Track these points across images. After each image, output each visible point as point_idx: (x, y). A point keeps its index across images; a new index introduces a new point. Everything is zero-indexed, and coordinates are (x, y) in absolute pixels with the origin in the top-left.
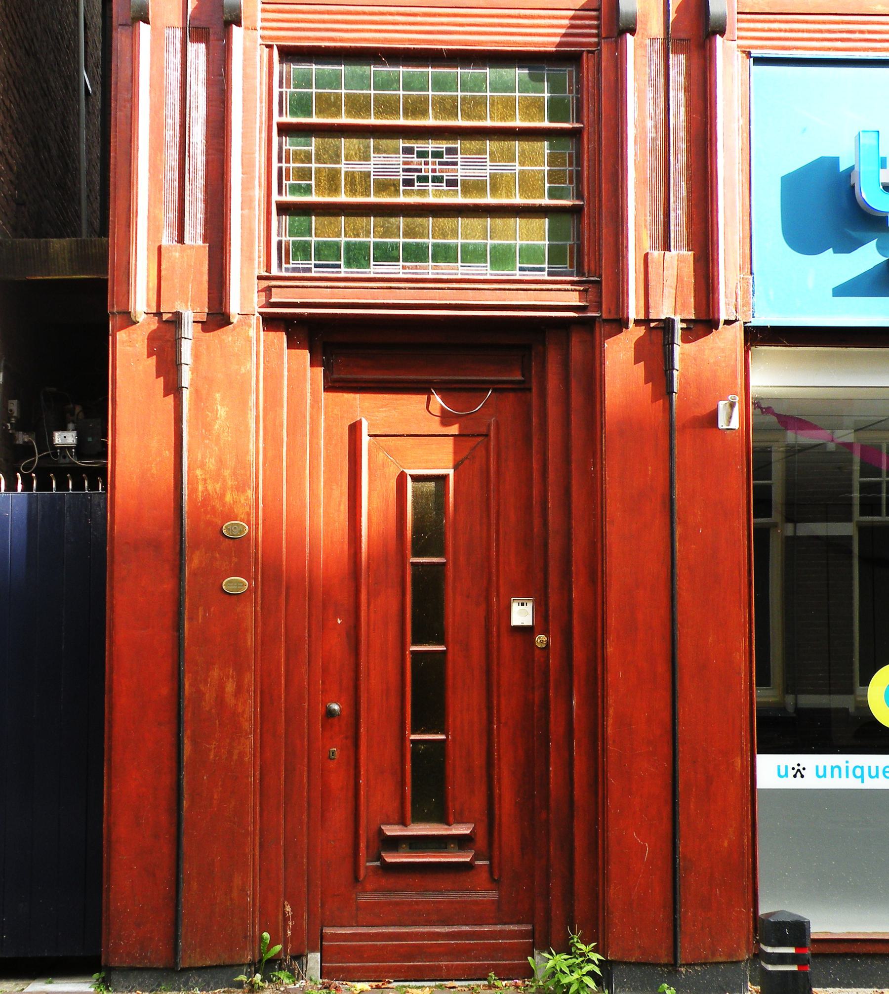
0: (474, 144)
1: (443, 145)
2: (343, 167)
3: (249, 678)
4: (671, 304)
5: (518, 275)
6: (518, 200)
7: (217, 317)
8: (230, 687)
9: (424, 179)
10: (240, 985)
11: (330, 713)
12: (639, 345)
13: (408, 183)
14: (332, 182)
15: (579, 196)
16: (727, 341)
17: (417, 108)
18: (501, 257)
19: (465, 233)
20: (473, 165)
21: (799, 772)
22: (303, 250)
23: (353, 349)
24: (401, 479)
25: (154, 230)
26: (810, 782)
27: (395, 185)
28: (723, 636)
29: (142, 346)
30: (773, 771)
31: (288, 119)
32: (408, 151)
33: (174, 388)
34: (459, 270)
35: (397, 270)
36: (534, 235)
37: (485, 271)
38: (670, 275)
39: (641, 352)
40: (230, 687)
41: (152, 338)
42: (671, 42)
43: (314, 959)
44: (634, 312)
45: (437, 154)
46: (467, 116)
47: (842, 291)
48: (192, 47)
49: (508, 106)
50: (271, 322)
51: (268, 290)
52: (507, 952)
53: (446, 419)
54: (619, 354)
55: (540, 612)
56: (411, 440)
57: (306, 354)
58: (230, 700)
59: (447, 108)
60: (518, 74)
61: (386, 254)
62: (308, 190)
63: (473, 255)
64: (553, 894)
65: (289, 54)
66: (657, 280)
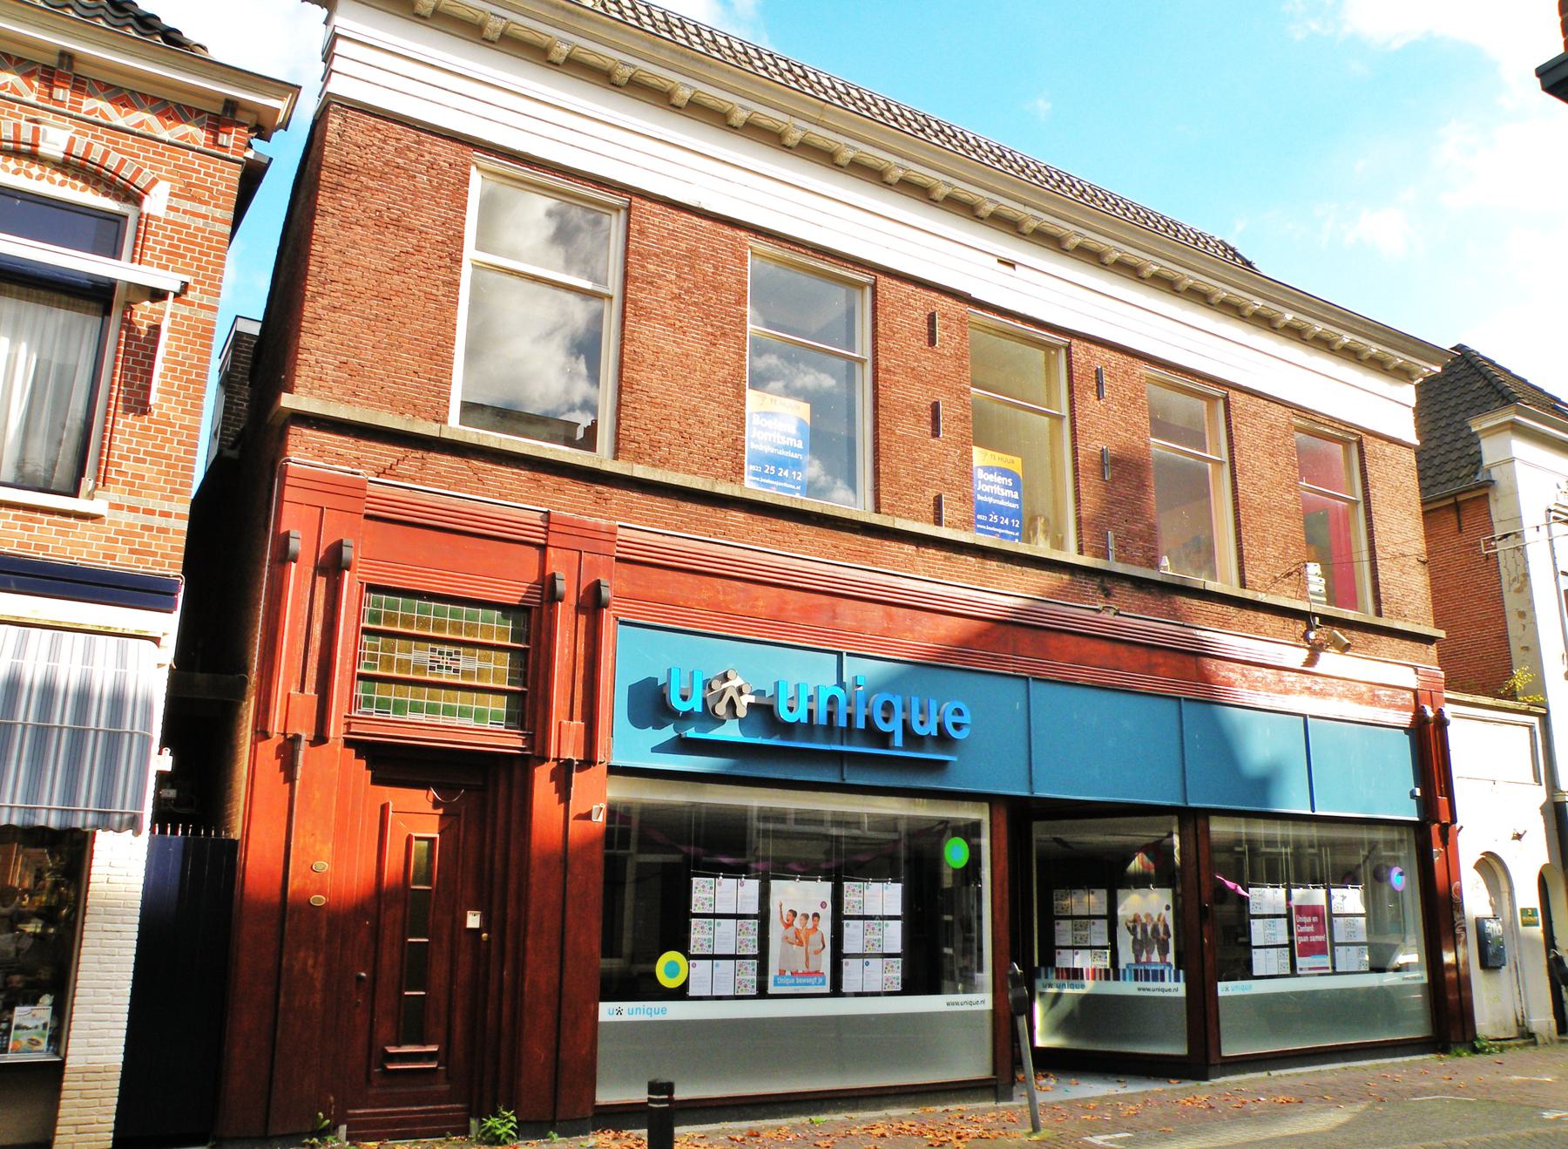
0: (471, 650)
1: (453, 649)
2: (397, 655)
3: (321, 958)
4: (572, 753)
5: (489, 727)
6: (491, 684)
7: (320, 738)
8: (310, 962)
9: (440, 667)
10: (304, 1145)
11: (360, 979)
12: (553, 771)
13: (432, 668)
14: (389, 663)
15: (525, 685)
16: (599, 771)
17: (439, 626)
18: (480, 715)
19: (460, 700)
20: (469, 662)
21: (619, 1012)
22: (369, 702)
23: (392, 762)
24: (409, 839)
25: (287, 685)
26: (625, 1017)
27: (424, 669)
28: (587, 934)
29: (272, 752)
30: (608, 1012)
31: (366, 625)
32: (433, 650)
33: (290, 778)
34: (457, 721)
35: (421, 718)
36: (499, 705)
37: (470, 722)
38: (572, 734)
39: (554, 776)
40: (310, 962)
41: (280, 749)
42: (579, 608)
43: (343, 1129)
44: (553, 755)
45: (449, 654)
46: (467, 634)
47: (656, 749)
48: (318, 578)
49: (490, 633)
50: (349, 743)
51: (349, 724)
52: (454, 1120)
53: (436, 805)
54: (542, 777)
55: (485, 920)
56: (417, 816)
57: (364, 762)
58: (310, 971)
59: (456, 628)
60: (497, 613)
61: (416, 708)
62: (375, 667)
63: (464, 713)
64: (480, 1083)
65: (372, 588)
66: (566, 739)
